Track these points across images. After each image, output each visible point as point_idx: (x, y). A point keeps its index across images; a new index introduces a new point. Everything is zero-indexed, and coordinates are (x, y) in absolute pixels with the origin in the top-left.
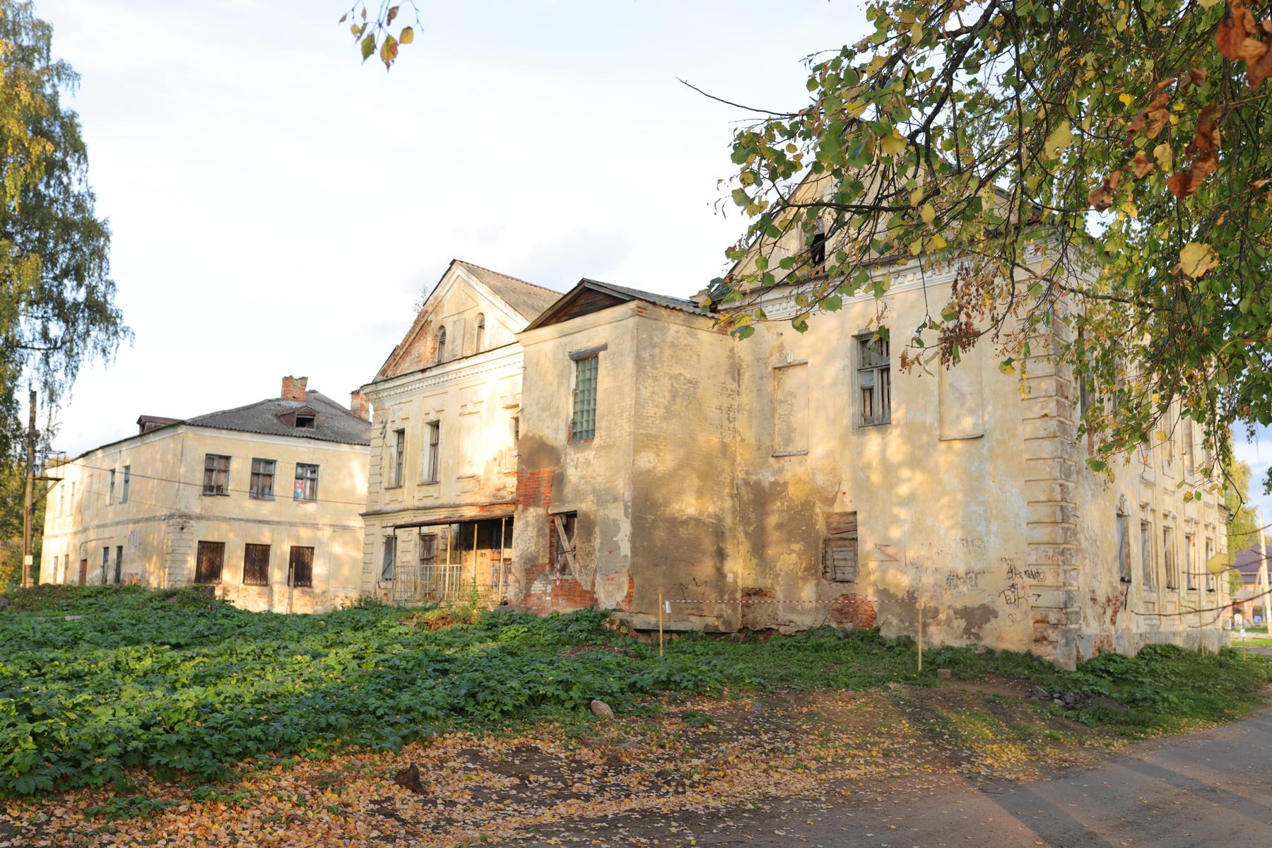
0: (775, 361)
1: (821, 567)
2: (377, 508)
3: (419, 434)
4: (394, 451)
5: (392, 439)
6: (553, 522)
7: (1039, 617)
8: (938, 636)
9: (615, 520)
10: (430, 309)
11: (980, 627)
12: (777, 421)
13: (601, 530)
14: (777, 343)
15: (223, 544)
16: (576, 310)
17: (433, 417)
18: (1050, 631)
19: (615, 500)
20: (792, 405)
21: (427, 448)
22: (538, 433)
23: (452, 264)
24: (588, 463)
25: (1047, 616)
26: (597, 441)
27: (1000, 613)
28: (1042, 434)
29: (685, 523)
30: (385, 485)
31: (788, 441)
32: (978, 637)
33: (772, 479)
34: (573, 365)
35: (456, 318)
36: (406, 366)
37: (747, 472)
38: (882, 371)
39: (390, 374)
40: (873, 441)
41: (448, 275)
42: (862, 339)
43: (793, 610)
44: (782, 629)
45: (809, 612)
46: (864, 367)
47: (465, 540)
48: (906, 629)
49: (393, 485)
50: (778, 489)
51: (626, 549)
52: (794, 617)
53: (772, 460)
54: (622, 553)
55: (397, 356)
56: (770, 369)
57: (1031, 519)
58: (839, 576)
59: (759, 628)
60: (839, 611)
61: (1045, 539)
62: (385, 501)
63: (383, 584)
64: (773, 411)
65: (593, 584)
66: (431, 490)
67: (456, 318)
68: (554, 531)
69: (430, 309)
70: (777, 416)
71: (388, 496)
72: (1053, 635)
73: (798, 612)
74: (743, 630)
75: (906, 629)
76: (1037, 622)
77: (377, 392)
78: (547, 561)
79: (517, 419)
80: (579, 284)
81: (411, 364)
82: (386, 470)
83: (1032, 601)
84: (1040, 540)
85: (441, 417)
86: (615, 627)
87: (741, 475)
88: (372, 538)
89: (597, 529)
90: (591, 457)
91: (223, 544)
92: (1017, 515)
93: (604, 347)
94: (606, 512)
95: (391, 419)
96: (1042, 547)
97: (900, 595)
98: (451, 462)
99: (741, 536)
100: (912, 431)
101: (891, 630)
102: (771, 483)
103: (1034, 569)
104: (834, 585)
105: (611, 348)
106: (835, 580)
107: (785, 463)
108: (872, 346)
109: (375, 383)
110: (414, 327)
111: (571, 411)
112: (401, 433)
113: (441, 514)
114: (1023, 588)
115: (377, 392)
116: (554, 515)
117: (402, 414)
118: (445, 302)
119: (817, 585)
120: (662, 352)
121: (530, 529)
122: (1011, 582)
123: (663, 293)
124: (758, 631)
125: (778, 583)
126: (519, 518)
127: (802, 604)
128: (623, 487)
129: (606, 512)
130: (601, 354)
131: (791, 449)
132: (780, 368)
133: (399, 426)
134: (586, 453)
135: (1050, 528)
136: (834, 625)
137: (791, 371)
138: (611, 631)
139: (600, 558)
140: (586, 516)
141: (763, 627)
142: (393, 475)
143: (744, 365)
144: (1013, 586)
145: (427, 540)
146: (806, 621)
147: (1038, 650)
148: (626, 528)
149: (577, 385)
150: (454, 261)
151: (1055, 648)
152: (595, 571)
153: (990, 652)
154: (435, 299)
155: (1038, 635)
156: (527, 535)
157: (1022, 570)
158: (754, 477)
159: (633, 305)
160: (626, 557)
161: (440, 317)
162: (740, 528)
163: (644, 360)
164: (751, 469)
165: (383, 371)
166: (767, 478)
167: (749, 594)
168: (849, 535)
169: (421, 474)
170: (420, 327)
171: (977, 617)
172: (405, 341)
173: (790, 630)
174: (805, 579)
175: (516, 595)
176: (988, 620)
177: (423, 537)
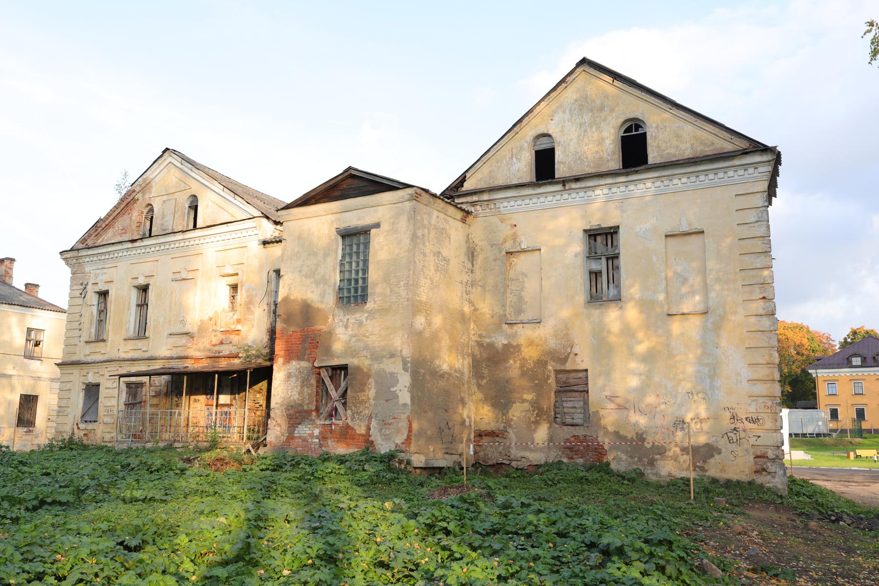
0: (508, 246)
1: (553, 413)
2: (75, 358)
3: (123, 298)
4: (95, 310)
5: (93, 299)
6: (319, 374)
7: (759, 454)
8: (670, 468)
9: (392, 374)
10: (137, 189)
11: (705, 462)
12: (508, 295)
13: (377, 383)
14: (512, 232)
15: (37, 396)
16: (337, 193)
17: (142, 281)
18: (769, 464)
19: (392, 356)
20: (523, 282)
21: (134, 308)
22: (304, 298)
23: (164, 152)
24: (360, 324)
25: (766, 453)
26: (370, 305)
27: (723, 450)
28: (761, 312)
29: (442, 376)
30: (85, 338)
31: (519, 311)
32: (703, 469)
33: (506, 342)
34: (340, 239)
35: (165, 198)
36: (109, 236)
37: (480, 336)
38: (607, 259)
39: (90, 242)
40: (612, 316)
41: (160, 161)
42: (592, 235)
43: (526, 448)
44: (514, 464)
45: (541, 450)
46: (592, 255)
47: (177, 388)
48: (634, 463)
49: (93, 339)
50: (510, 350)
51: (405, 397)
52: (527, 454)
53: (505, 327)
54: (401, 401)
55: (99, 228)
56: (504, 253)
57: (751, 378)
58: (568, 420)
59: (490, 463)
60: (570, 449)
61: (765, 393)
62: (83, 353)
63: (82, 426)
64: (506, 287)
65: (369, 428)
66: (140, 344)
67: (165, 198)
68: (321, 382)
69: (137, 189)
70: (508, 291)
71: (88, 349)
72: (772, 468)
73: (531, 450)
74: (476, 465)
75: (634, 463)
76: (757, 457)
77: (77, 258)
78: (314, 408)
79: (234, 287)
80: (345, 171)
81: (114, 235)
82: (86, 326)
83: (752, 441)
84: (760, 394)
85: (151, 281)
86: (403, 466)
87: (474, 338)
88: (69, 386)
89: (371, 380)
90: (363, 319)
91: (37, 396)
92: (738, 374)
93: (377, 225)
94: (382, 366)
95: (92, 281)
96: (761, 400)
97: (629, 437)
98: (161, 320)
99: (474, 388)
100: (646, 305)
101: (619, 461)
102: (505, 345)
103: (754, 416)
104: (565, 428)
105: (385, 226)
106: (565, 424)
107: (518, 328)
108: (602, 240)
109: (72, 250)
110: (119, 204)
111: (338, 279)
112: (104, 294)
113: (157, 366)
114: (744, 431)
115: (77, 258)
116: (320, 367)
117: (105, 278)
118: (153, 184)
119: (550, 428)
120: (429, 233)
121: (294, 379)
122: (733, 426)
123: (301, 195)
124: (490, 466)
125: (510, 426)
126: (279, 371)
127: (538, 443)
128: (400, 343)
129: (382, 366)
130: (373, 231)
131: (523, 317)
132: (511, 253)
133: (102, 287)
134: (358, 315)
135: (768, 385)
136: (565, 460)
137: (523, 256)
138: (401, 470)
139: (375, 405)
140: (358, 369)
141: (495, 462)
142: (93, 330)
143: (478, 248)
144: (735, 429)
145: (133, 389)
146: (536, 457)
147: (760, 479)
148: (405, 379)
149: (343, 256)
150: (167, 149)
151: (773, 477)
152: (370, 417)
153: (714, 481)
154: (144, 180)
155: (758, 467)
156: (284, 384)
157: (744, 417)
158: (488, 340)
159: (409, 191)
160: (405, 405)
161: (147, 196)
162: (474, 381)
163: (418, 237)
164: (484, 333)
165: (83, 240)
166: (500, 341)
167: (480, 436)
168: (580, 388)
169: (128, 330)
170: (127, 203)
171: (703, 454)
172: (109, 215)
173: (521, 464)
174: (537, 423)
175: (276, 437)
176: (712, 456)
177: (128, 385)
